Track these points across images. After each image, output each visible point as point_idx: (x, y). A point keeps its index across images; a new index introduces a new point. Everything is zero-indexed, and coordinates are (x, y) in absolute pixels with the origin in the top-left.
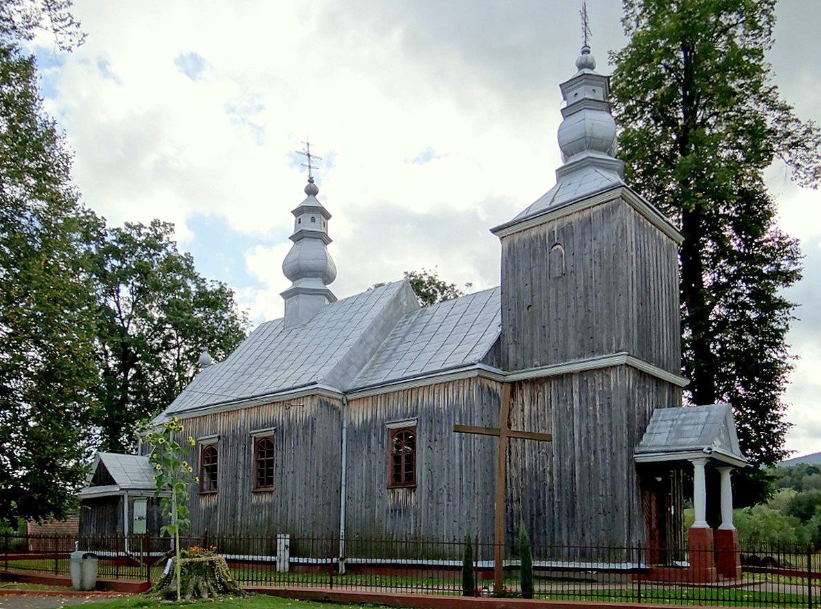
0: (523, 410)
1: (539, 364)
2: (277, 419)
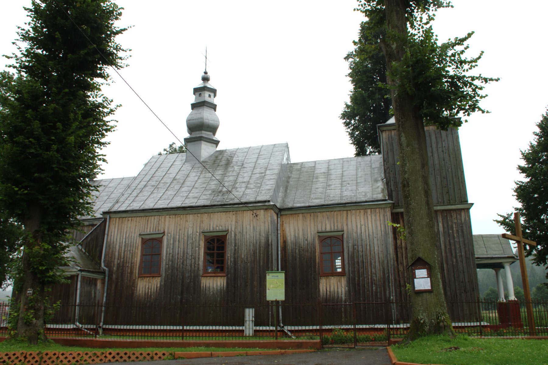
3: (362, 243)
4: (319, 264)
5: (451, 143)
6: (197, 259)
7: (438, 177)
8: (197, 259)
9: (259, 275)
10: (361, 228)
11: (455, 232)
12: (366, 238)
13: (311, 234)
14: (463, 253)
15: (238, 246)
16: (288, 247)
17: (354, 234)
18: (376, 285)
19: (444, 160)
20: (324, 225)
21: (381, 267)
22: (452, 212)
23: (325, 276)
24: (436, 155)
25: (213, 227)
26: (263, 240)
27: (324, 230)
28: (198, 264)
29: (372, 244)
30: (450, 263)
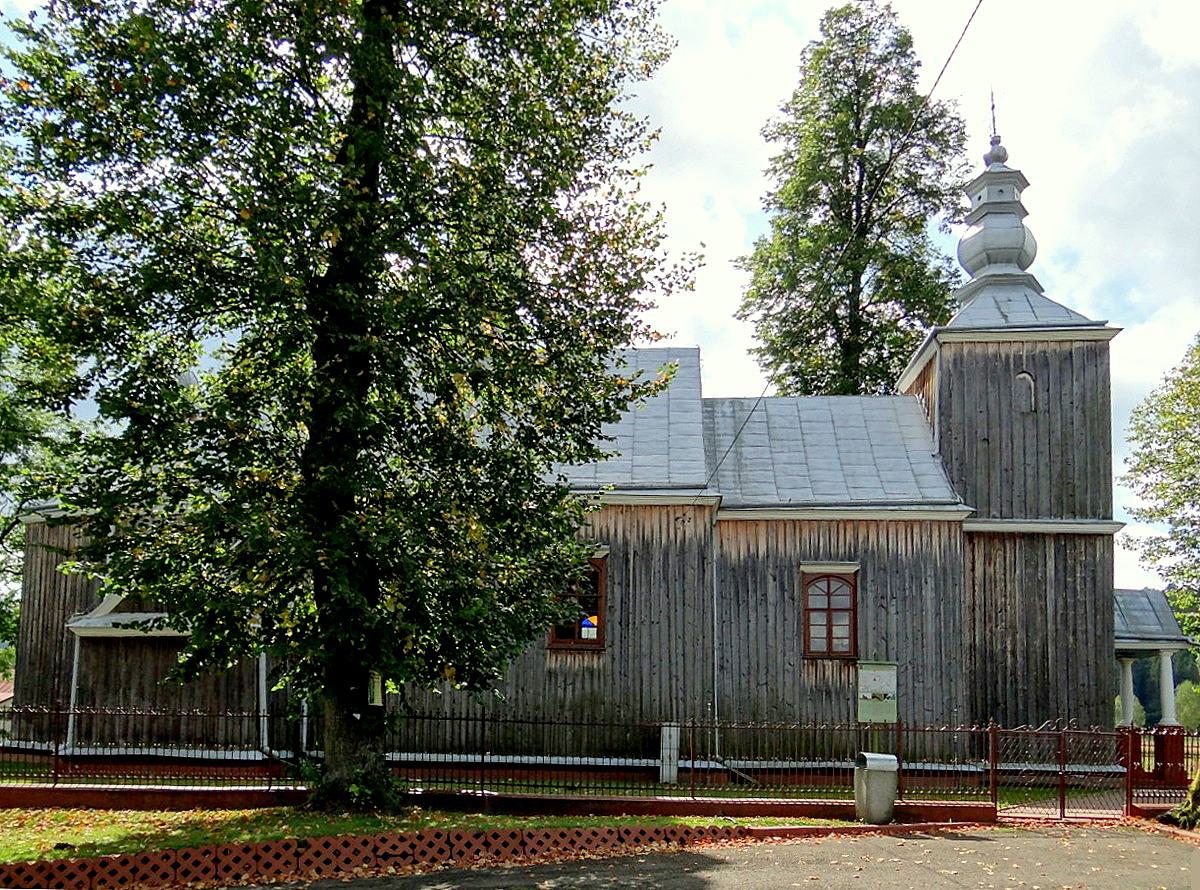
0: (973, 570)
1: (998, 515)
2: (612, 532)
11: (1078, 581)
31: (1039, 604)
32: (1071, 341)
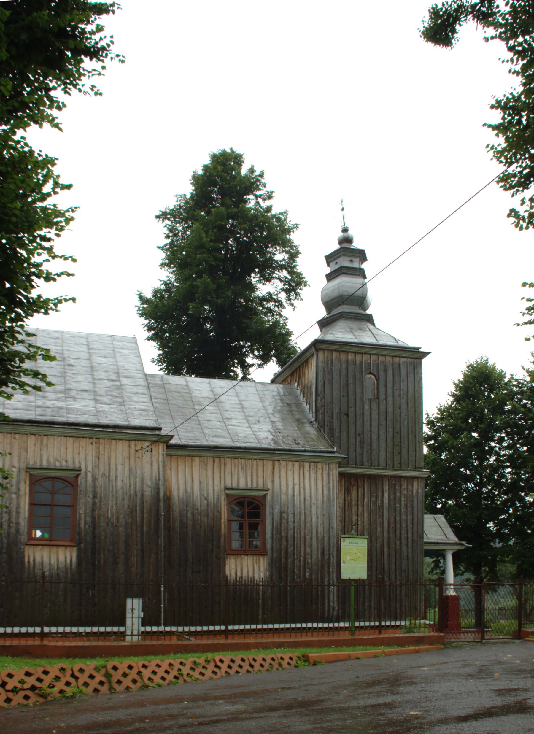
3: (294, 510)
4: (225, 536)
5: (411, 386)
6: (14, 514)
7: (390, 430)
8: (14, 514)
9: (139, 547)
10: (294, 488)
11: (403, 506)
12: (300, 504)
13: (214, 491)
14: (410, 535)
15: (101, 497)
16: (174, 508)
17: (283, 496)
18: (311, 570)
19: (400, 408)
20: (235, 478)
21: (320, 546)
22: (402, 480)
23: (233, 555)
24: (390, 399)
25: (48, 461)
26: (148, 492)
27: (235, 485)
28: (18, 524)
29: (308, 512)
30: (392, 545)
31: (379, 520)
32: (399, 357)
